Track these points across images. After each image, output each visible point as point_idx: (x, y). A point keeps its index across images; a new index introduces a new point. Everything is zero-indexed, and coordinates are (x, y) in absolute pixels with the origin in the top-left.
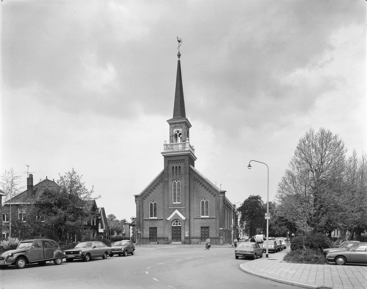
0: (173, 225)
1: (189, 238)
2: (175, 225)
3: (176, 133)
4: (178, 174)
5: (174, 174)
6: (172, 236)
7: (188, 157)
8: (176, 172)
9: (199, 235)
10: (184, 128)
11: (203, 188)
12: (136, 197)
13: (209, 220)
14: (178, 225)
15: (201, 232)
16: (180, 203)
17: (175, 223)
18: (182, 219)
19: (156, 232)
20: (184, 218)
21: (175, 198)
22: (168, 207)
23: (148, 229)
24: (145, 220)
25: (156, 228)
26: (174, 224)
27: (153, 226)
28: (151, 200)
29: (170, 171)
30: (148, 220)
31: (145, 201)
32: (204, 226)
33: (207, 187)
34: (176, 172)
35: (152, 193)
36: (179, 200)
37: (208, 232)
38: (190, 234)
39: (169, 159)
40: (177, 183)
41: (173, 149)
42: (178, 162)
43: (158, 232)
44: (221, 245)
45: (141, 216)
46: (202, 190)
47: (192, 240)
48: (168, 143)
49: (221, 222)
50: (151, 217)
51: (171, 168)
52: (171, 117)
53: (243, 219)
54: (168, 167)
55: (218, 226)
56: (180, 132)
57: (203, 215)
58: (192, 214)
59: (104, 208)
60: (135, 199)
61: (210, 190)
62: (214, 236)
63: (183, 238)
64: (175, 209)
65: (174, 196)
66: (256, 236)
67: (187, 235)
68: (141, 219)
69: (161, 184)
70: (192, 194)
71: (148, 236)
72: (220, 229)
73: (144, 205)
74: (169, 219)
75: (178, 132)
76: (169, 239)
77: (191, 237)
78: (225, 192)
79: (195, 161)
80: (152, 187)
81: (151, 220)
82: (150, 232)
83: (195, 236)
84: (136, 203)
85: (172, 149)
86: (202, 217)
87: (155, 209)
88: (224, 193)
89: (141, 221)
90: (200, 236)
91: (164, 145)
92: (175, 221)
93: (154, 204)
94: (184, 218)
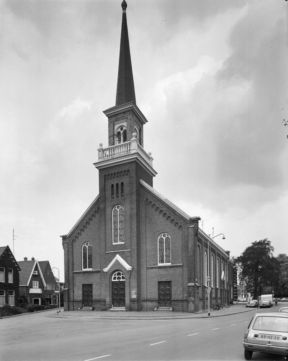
0: (113, 280)
1: (139, 300)
2: (116, 280)
3: (119, 130)
4: (120, 196)
5: (115, 195)
6: (112, 297)
7: (135, 166)
8: (117, 193)
9: (155, 295)
10: (130, 119)
11: (161, 216)
12: (64, 238)
13: (171, 271)
14: (121, 280)
15: (159, 290)
16: (123, 243)
17: (116, 276)
18: (126, 269)
19: (91, 292)
20: (128, 267)
21: (116, 236)
22: (106, 252)
23: (81, 286)
24: (76, 273)
25: (92, 285)
26: (115, 278)
27: (87, 283)
28: (83, 241)
29: (108, 192)
30: (80, 273)
31: (76, 244)
32: (163, 280)
33: (168, 213)
34: (117, 193)
35: (86, 230)
36: (121, 238)
37: (170, 290)
38: (139, 293)
39: (107, 173)
40: (118, 210)
41: (114, 154)
42: (120, 176)
43: (93, 291)
44: (192, 312)
45: (71, 268)
46: (159, 219)
47: (145, 304)
48: (106, 145)
49: (191, 273)
50: (84, 268)
51: (109, 187)
52: (113, 104)
53: (244, 273)
54: (105, 187)
55: (186, 280)
56: (124, 128)
57: (162, 261)
58: (143, 260)
59: (48, 261)
60: (63, 242)
61: (172, 218)
62: (180, 297)
63: (127, 301)
64: (116, 253)
65: (114, 232)
66: (262, 296)
67: (134, 296)
68: (70, 272)
69: (97, 216)
70: (143, 228)
71: (81, 298)
72: (190, 284)
73: (75, 250)
74: (106, 270)
75: (122, 129)
76: (107, 302)
77: (142, 299)
78: (199, 221)
79: (154, 178)
80: (85, 222)
81: (84, 272)
82: (83, 291)
83: (149, 297)
84: (64, 248)
85: (111, 156)
86: (160, 265)
87: (90, 257)
88: (196, 220)
89: (71, 275)
90: (157, 297)
91: (99, 150)
92: (117, 273)
93: (89, 247)
94: (128, 267)
